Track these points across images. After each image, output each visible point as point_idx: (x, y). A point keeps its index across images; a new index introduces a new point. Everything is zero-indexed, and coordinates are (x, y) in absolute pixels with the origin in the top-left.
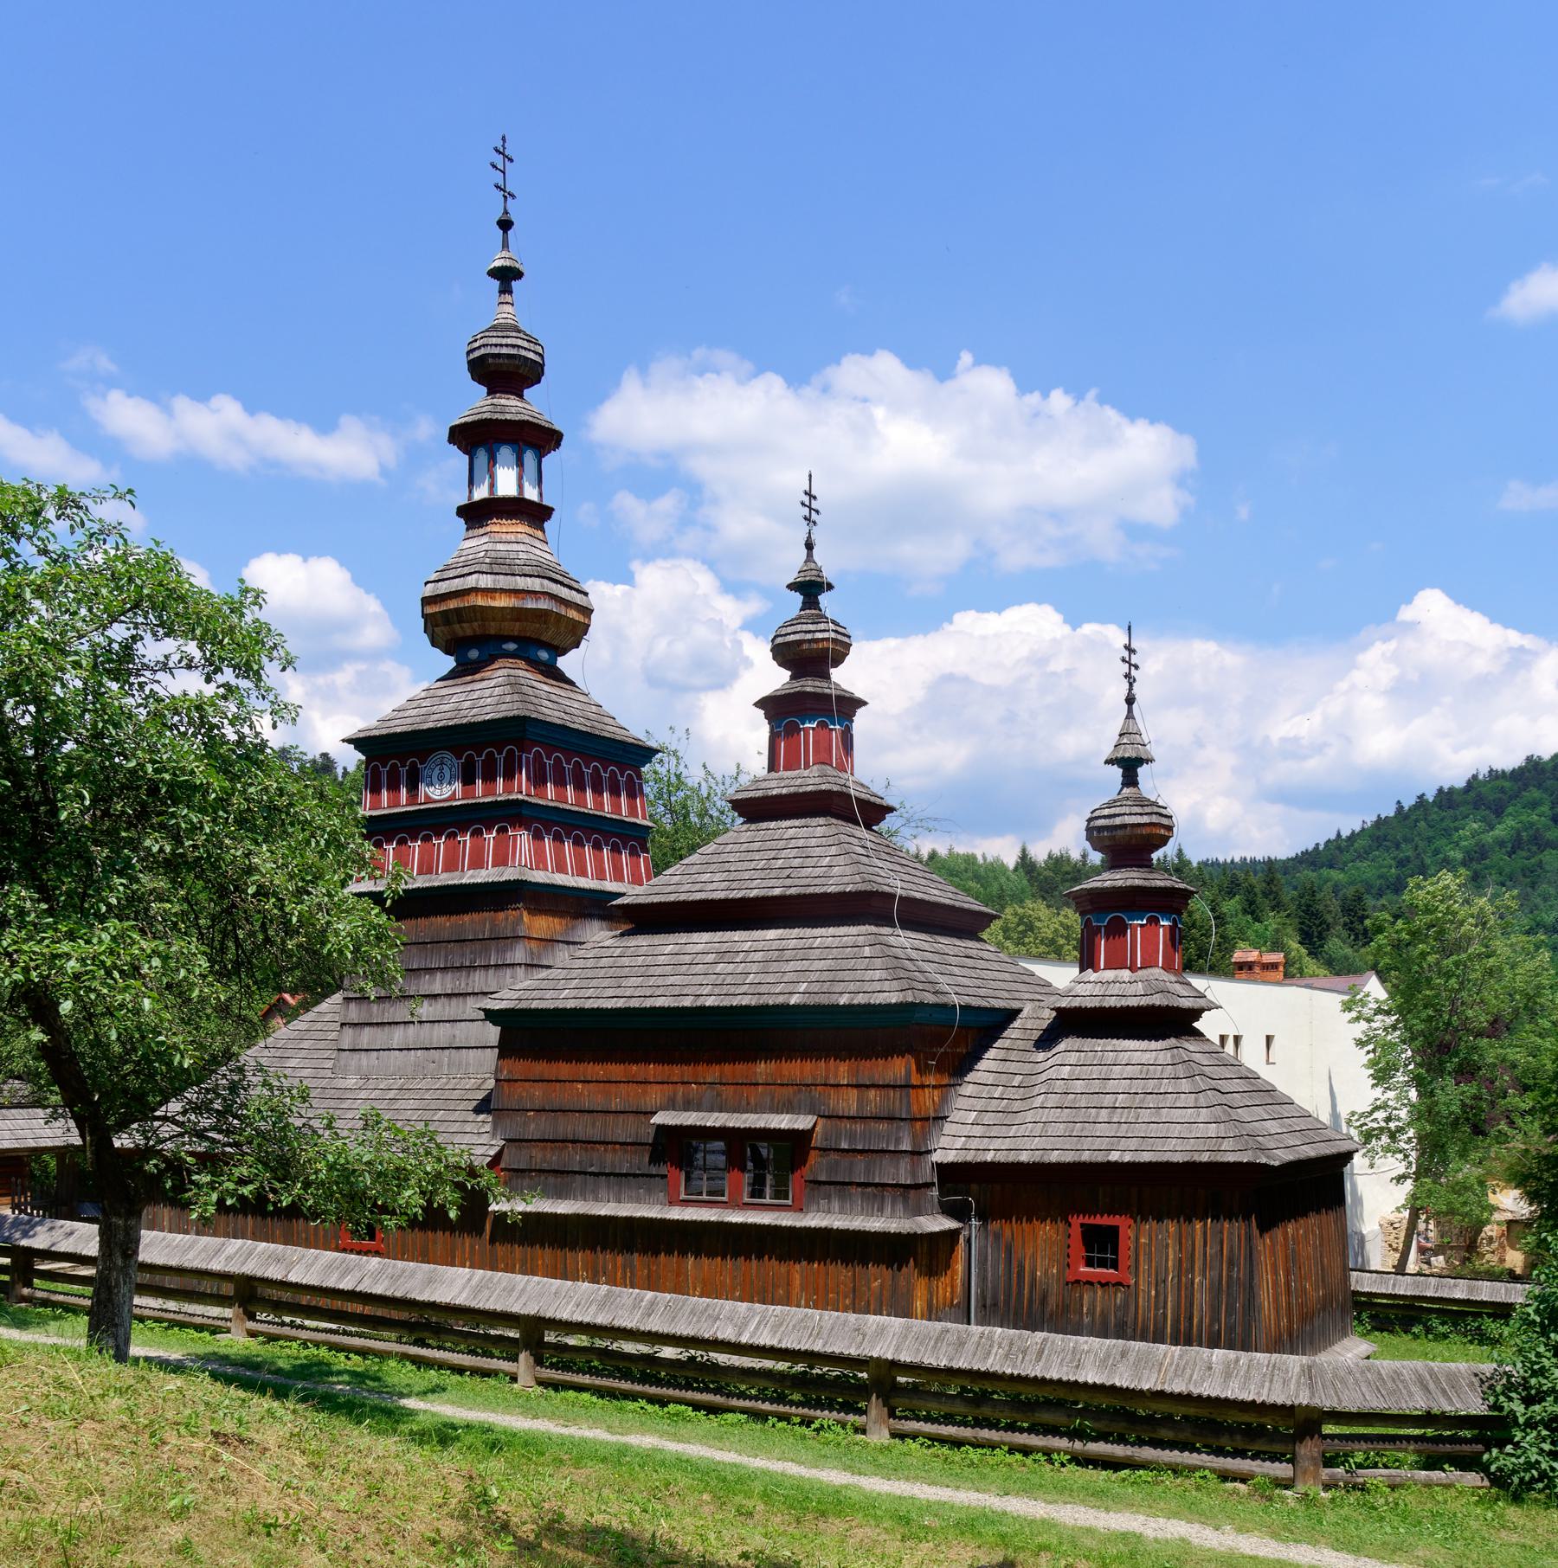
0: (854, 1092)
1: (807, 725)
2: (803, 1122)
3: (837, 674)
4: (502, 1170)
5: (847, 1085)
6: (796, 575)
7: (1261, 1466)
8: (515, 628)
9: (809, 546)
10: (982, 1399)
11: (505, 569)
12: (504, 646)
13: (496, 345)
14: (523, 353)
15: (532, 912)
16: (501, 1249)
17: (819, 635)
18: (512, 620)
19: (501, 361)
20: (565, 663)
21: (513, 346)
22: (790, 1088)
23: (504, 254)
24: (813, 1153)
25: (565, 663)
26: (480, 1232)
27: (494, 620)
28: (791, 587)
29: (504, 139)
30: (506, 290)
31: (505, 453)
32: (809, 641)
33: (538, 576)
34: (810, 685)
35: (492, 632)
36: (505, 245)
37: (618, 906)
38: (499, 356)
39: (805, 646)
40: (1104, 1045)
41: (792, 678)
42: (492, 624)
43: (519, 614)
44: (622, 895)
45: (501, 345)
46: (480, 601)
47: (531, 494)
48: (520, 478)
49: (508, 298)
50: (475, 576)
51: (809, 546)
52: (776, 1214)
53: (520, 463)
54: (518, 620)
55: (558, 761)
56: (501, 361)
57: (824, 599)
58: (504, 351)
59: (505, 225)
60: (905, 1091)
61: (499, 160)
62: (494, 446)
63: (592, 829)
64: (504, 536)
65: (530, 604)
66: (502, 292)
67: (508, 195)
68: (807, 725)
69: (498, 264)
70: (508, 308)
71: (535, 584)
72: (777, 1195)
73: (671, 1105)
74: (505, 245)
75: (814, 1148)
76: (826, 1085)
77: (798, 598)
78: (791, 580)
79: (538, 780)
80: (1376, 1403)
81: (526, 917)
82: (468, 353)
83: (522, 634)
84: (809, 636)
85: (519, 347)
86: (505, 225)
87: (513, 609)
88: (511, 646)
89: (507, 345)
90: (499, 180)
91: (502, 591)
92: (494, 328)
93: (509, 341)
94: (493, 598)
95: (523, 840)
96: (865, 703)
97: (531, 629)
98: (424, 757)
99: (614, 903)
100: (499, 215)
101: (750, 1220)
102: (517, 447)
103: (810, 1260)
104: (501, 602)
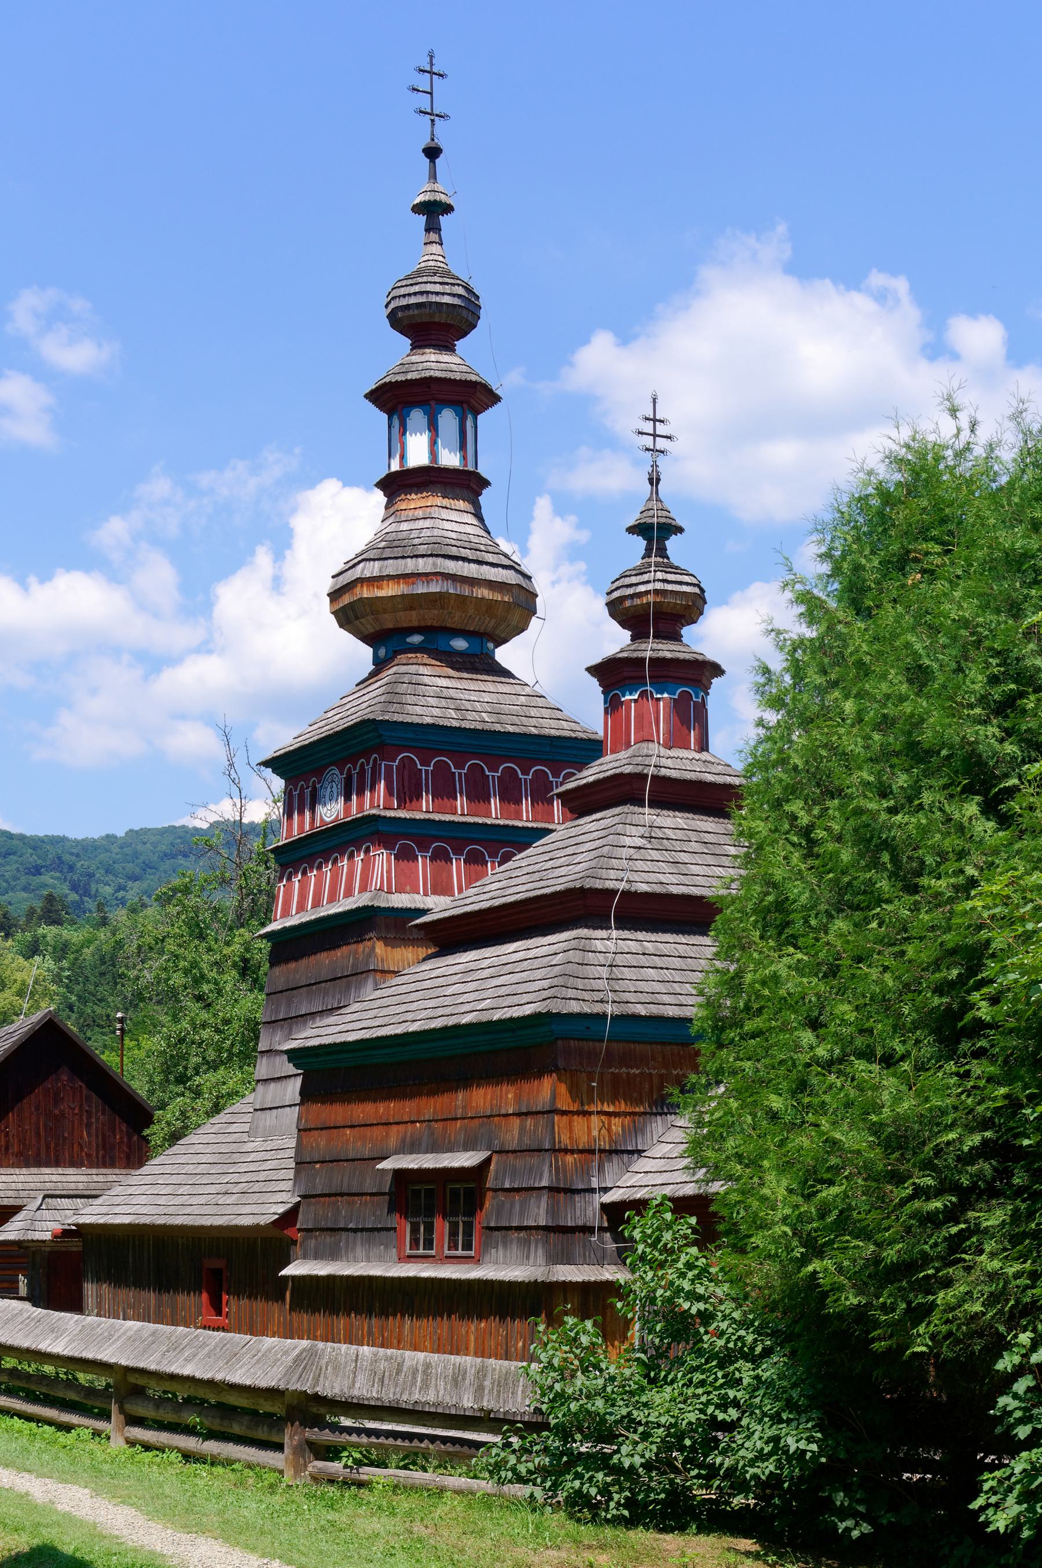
0: (516, 1122)
1: (628, 697)
2: (466, 1160)
3: (688, 632)
4: (299, 1230)
5: (513, 1114)
6: (638, 516)
7: (273, 1458)
8: (413, 618)
9: (654, 480)
10: (138, 1392)
11: (398, 552)
12: (409, 640)
13: (404, 296)
14: (434, 299)
15: (387, 942)
16: (304, 1319)
17: (642, 588)
18: (405, 610)
19: (411, 312)
20: (504, 655)
21: (421, 293)
22: (476, 1121)
24: (489, 1194)
25: (504, 655)
26: (283, 1299)
27: (385, 611)
28: (631, 530)
30: (432, 227)
31: (417, 417)
32: (632, 596)
33: (431, 555)
34: (652, 649)
35: (390, 626)
36: (433, 176)
37: (417, 926)
38: (407, 307)
39: (628, 603)
40: (422, 1025)
41: (634, 638)
42: (386, 616)
43: (411, 602)
44: (424, 912)
45: (409, 295)
46: (366, 593)
47: (450, 459)
48: (433, 443)
49: (433, 237)
50: (361, 565)
51: (654, 480)
52: (420, 1266)
53: (433, 427)
54: (412, 608)
55: (407, 763)
56: (411, 312)
57: (673, 544)
58: (413, 300)
59: (432, 153)
60: (550, 1115)
61: (423, 82)
62: (405, 410)
63: (498, 841)
64: (411, 513)
65: (421, 589)
66: (428, 230)
67: (433, 116)
68: (628, 697)
69: (417, 201)
70: (435, 248)
71: (423, 565)
72: (467, 1246)
73: (412, 1147)
74: (433, 176)
75: (489, 1189)
76: (499, 1115)
77: (639, 543)
78: (632, 522)
79: (408, 794)
80: (389, 1395)
81: (380, 948)
82: (387, 306)
83: (423, 624)
84: (630, 591)
85: (427, 293)
86: (432, 153)
87: (403, 596)
88: (416, 639)
89: (415, 294)
90: (423, 101)
91: (390, 577)
92: (419, 273)
93: (416, 288)
94: (379, 587)
95: (382, 860)
96: (589, 669)
97: (432, 617)
98: (319, 772)
99: (418, 921)
100: (425, 141)
101: (425, 1274)
102: (459, 408)
103: (480, 1318)
104: (389, 590)
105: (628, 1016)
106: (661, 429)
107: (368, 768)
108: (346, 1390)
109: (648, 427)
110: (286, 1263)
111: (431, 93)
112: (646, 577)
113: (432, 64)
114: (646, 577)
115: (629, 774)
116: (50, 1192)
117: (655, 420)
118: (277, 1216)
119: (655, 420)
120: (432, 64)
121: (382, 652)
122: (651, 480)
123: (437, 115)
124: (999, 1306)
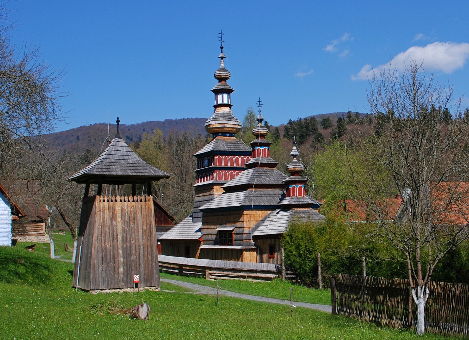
12: (219, 134)
23: (222, 54)
29: (221, 31)
36: (222, 52)
59: (222, 48)
86: (222, 48)
88: (220, 134)
105: (255, 205)
106: (260, 103)
107: (212, 158)
108: (57, 105)
109: (258, 103)
110: (200, 246)
111: (221, 37)
112: (258, 129)
113: (221, 32)
114: (258, 129)
115: (256, 163)
116: (229, 264)
117: (259, 102)
118: (285, 199)
119: (259, 102)
120: (221, 32)
121: (214, 136)
122: (259, 112)
123: (223, 41)
124: (455, 279)
